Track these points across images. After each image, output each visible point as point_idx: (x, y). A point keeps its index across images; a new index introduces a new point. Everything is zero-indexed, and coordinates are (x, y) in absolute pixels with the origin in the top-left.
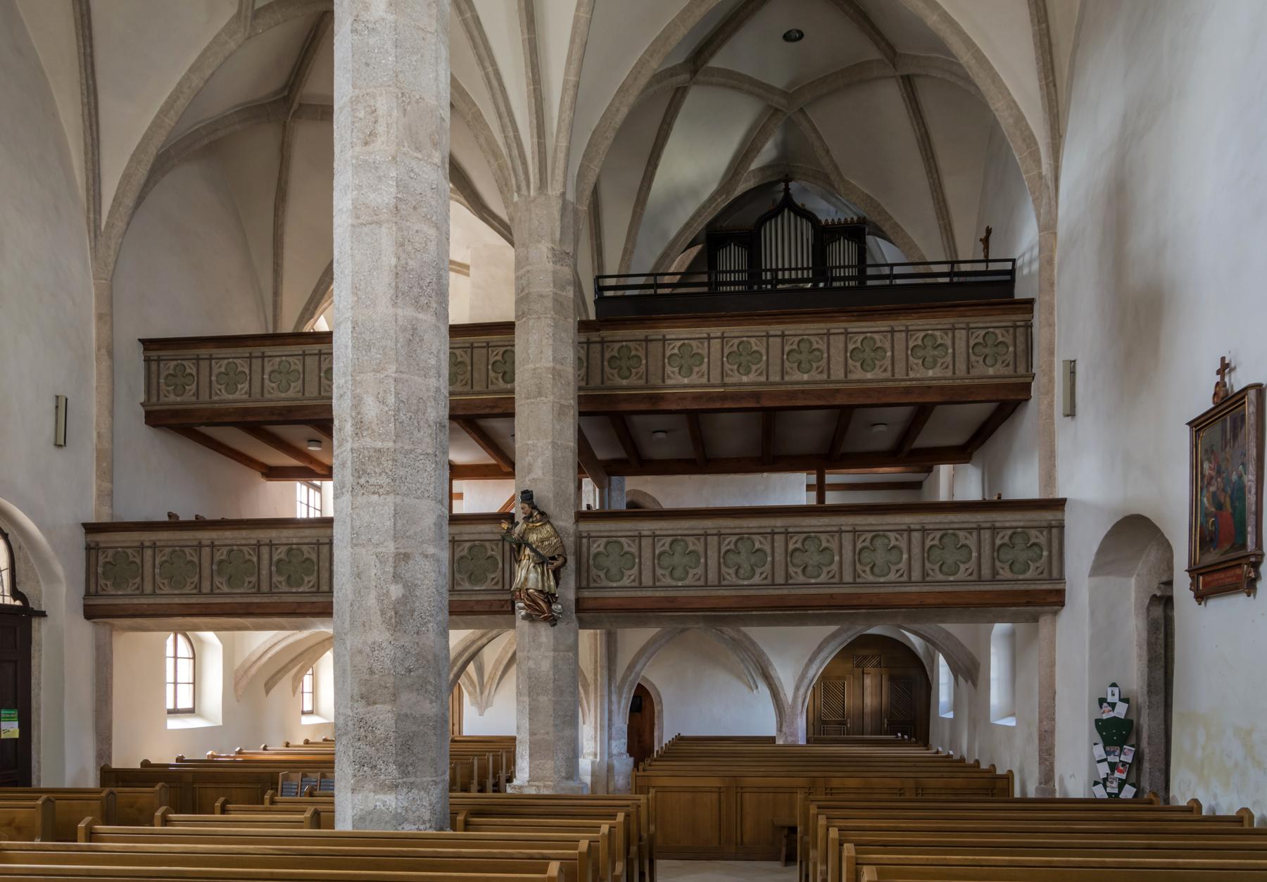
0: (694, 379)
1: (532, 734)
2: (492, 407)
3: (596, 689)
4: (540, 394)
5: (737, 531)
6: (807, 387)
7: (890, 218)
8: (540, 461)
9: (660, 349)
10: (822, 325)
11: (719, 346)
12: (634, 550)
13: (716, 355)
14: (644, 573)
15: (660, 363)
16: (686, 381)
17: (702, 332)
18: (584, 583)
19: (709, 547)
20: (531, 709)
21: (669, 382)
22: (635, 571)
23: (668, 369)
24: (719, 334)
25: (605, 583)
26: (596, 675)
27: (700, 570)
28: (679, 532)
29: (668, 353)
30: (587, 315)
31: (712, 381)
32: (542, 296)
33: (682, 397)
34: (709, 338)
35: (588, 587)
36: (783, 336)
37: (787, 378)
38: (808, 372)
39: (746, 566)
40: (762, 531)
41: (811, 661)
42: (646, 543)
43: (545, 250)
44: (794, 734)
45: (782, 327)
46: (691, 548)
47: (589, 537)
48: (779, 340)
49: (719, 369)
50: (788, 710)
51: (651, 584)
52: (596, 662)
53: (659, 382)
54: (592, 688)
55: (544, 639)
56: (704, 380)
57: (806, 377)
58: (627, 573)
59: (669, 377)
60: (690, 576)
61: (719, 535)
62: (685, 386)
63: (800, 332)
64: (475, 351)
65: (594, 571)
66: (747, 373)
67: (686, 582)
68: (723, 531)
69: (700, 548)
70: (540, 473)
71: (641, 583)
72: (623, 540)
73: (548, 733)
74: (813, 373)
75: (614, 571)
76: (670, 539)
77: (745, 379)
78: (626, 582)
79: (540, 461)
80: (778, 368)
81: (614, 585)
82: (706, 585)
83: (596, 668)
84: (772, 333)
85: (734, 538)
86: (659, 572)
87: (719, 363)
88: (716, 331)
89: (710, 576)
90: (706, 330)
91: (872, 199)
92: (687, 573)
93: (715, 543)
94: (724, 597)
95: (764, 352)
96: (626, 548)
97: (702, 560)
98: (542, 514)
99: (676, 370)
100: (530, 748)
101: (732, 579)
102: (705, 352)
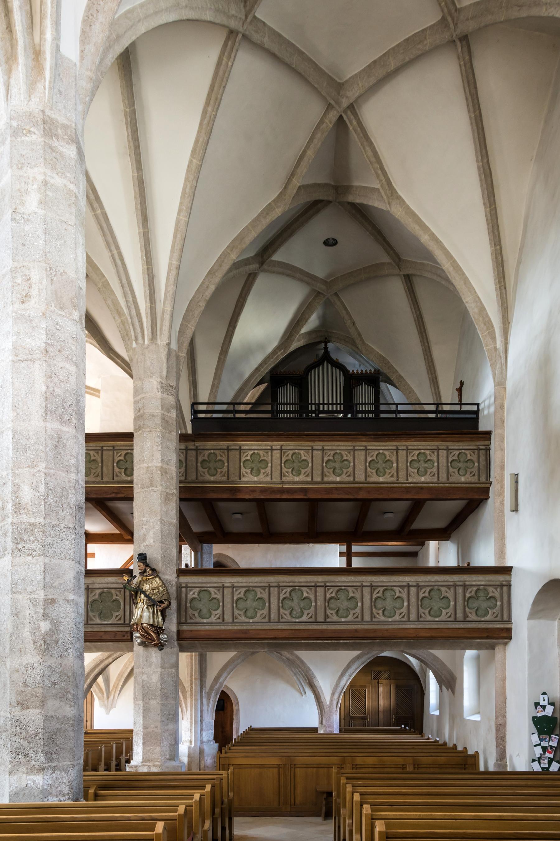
0: (261, 478)
4: (151, 485)
6: (339, 486)
8: (151, 533)
9: (238, 456)
10: (349, 444)
12: (219, 596)
14: (226, 612)
16: (256, 479)
17: (267, 445)
18: (183, 620)
20: (144, 710)
21: (244, 479)
22: (219, 611)
23: (243, 470)
25: (198, 619)
26: (191, 684)
27: (265, 611)
28: (251, 584)
32: (153, 416)
33: (253, 490)
34: (272, 450)
35: (186, 622)
36: (323, 450)
37: (326, 479)
39: (297, 608)
40: (309, 584)
43: (155, 383)
44: (331, 726)
45: (322, 444)
46: (259, 595)
47: (187, 587)
48: (320, 453)
49: (279, 472)
51: (231, 620)
52: (192, 675)
54: (188, 694)
55: (154, 660)
56: (268, 479)
57: (338, 479)
58: (214, 613)
59: (244, 476)
60: (259, 615)
63: (334, 448)
64: (104, 452)
65: (190, 612)
66: (299, 475)
68: (281, 584)
69: (265, 596)
71: (223, 619)
72: (211, 590)
73: (156, 727)
74: (344, 476)
75: (204, 611)
77: (297, 479)
78: (213, 619)
79: (151, 533)
80: (320, 472)
84: (315, 447)
86: (237, 612)
87: (279, 467)
88: (277, 445)
89: (272, 616)
91: (384, 358)
92: (256, 613)
96: (214, 595)
97: (267, 604)
99: (249, 471)
101: (288, 618)
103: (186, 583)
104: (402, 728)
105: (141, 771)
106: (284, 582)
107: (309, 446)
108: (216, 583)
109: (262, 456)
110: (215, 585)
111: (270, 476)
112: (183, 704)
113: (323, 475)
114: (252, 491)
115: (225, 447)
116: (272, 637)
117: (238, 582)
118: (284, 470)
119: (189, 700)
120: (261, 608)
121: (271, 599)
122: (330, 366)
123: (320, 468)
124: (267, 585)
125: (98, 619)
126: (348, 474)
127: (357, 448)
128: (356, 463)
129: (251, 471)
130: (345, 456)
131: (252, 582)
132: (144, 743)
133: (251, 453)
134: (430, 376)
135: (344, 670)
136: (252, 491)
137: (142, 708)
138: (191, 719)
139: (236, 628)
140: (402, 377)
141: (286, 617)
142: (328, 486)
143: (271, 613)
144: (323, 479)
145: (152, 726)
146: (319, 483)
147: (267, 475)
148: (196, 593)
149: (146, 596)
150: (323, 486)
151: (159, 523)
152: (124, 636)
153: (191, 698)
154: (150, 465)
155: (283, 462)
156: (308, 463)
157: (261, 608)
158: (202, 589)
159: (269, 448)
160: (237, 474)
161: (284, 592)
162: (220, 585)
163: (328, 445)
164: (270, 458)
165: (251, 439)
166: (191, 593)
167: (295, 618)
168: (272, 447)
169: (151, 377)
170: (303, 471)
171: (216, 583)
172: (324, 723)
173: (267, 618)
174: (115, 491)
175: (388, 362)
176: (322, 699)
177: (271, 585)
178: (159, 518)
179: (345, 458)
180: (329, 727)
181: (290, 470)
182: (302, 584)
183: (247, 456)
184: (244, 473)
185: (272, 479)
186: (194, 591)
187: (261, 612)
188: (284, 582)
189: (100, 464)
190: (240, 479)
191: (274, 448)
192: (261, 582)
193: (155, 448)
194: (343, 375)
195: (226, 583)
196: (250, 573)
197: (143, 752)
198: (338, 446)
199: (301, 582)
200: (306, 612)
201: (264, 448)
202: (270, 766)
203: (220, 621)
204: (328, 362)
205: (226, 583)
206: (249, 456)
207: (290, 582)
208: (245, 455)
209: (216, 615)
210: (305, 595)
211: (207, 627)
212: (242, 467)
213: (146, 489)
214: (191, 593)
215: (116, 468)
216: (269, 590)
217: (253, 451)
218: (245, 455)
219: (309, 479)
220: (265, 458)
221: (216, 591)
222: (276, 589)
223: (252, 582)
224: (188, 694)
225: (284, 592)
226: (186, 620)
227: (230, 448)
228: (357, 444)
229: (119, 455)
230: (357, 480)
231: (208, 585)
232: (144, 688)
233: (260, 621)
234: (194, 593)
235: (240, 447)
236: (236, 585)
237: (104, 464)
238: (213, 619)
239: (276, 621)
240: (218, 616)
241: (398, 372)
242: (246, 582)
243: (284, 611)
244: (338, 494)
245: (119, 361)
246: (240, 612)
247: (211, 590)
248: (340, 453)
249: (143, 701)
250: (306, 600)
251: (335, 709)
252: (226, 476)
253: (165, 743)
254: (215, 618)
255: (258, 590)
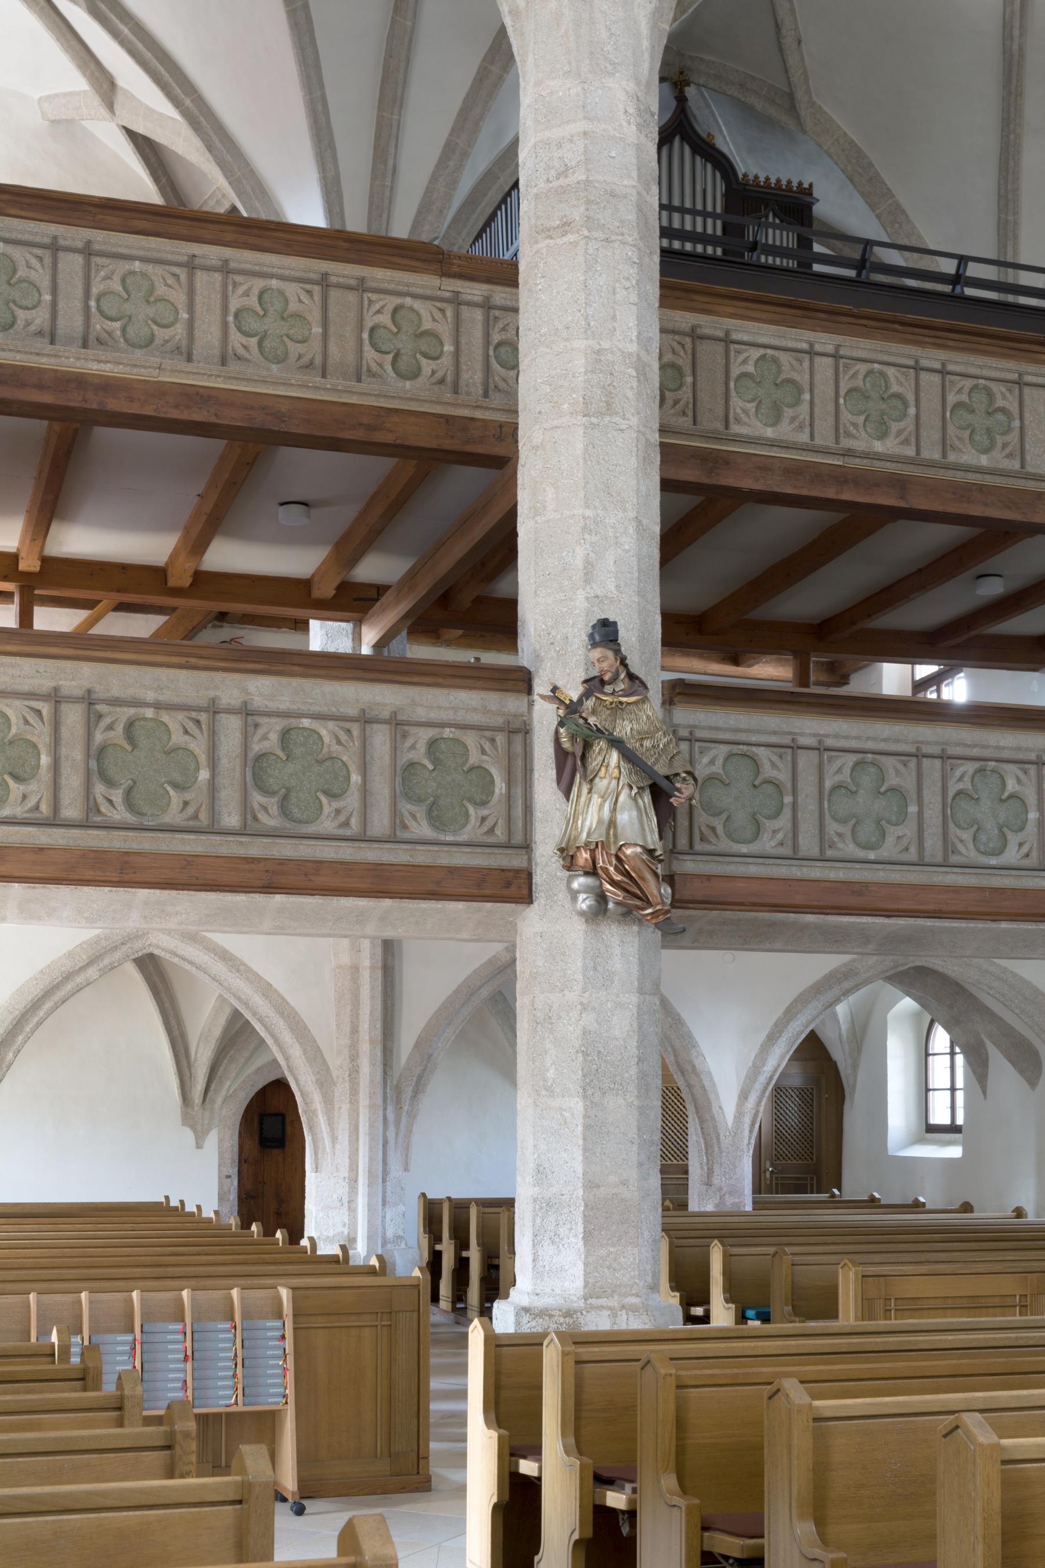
0: (784, 431)
1: (590, 1185)
2: (370, 428)
3: (354, 1092)
4: (609, 409)
5: (976, 752)
6: (989, 480)
7: (890, 194)
8: (610, 558)
9: (720, 360)
10: (1011, 364)
11: (830, 373)
12: (783, 776)
13: (825, 390)
14: (803, 827)
15: (720, 390)
16: (769, 433)
17: (799, 337)
18: (683, 842)
19: (926, 783)
20: (587, 1127)
21: (735, 428)
22: (784, 821)
23: (737, 403)
24: (830, 349)
25: (725, 844)
26: (354, 1058)
27: (908, 830)
28: (870, 745)
29: (735, 371)
30: (1005, 254)
31: (819, 441)
32: (613, 194)
33: (765, 466)
34: (812, 353)
35: (691, 850)
36: (943, 372)
37: (952, 457)
38: (986, 451)
39: (990, 825)
40: (1021, 756)
41: (772, 1038)
42: (806, 761)
43: (621, 95)
44: (735, 1191)
45: (942, 355)
46: (892, 780)
47: (691, 740)
48: (936, 378)
49: (831, 420)
50: (726, 1142)
51: (815, 852)
52: (355, 1030)
53: (719, 426)
54: (341, 1090)
55: (617, 965)
56: (804, 437)
57: (984, 460)
58: (770, 825)
59: (738, 421)
60: (890, 840)
61: (943, 757)
62: (772, 444)
63: (972, 371)
64: (334, 293)
65: (702, 818)
66: (883, 436)
67: (884, 853)
68: (951, 751)
69: (909, 783)
70: (611, 586)
71: (795, 847)
72: (762, 752)
73: (624, 1183)
74: (997, 454)
75: (741, 818)
76: (853, 758)
77: (878, 447)
78: (767, 844)
79: (610, 558)
80: (937, 436)
81: (744, 849)
82: (921, 863)
83: (354, 1046)
84: (924, 363)
85: (971, 767)
86: (832, 827)
87: (831, 407)
88: (826, 342)
89: (928, 843)
90: (808, 335)
91: (859, 151)
92: (883, 835)
93: (937, 775)
94: (957, 890)
95: (911, 397)
96: (768, 772)
97: (913, 809)
98: (632, 677)
99: (751, 406)
100: (587, 1220)
101: (969, 853)
102: (804, 379)
103: (692, 728)
104: (833, 1195)
105: (592, 1327)
106: (957, 744)
107: (909, 357)
108: (775, 733)
109: (786, 367)
110: (773, 739)
111: (807, 430)
112: (322, 1120)
113: (945, 446)
114: (760, 468)
115: (685, 326)
116: (931, 907)
117: (836, 736)
118: (846, 416)
119: (344, 1109)
120: (894, 818)
121: (926, 792)
122: (687, 150)
123: (938, 423)
124: (912, 749)
125: (424, 823)
126: (1007, 451)
127: (1028, 378)
128: (1027, 422)
129: (757, 408)
130: (999, 396)
131: (874, 739)
132: (588, 1236)
133: (756, 353)
134: (1011, 218)
135: (776, 1025)
136: (760, 468)
137: (580, 1121)
138: (353, 1167)
139: (832, 875)
140: (903, 212)
141: (963, 850)
142: (959, 476)
143: (926, 834)
144: (944, 455)
145: (613, 1179)
146: (931, 464)
147: (801, 427)
148: (719, 762)
149: (628, 756)
150: (949, 475)
151: (631, 531)
152: (508, 885)
153: (354, 1101)
154: (606, 344)
155: (842, 393)
156: (906, 404)
157: (894, 818)
158: (736, 749)
159: (805, 346)
160: (720, 410)
161: (958, 773)
162: (786, 740)
163: (960, 361)
164: (807, 377)
165: (758, 315)
166: (705, 760)
167: (984, 853)
168: (811, 345)
169: (611, 74)
170: (895, 427)
171: (775, 733)
172: (716, 1180)
173: (913, 850)
174: (365, 421)
175: (871, 164)
176: (715, 1109)
177: (925, 749)
178: (632, 514)
179: (1000, 403)
180: (730, 1193)
181: (862, 418)
182: (1006, 754)
183: (745, 362)
184: (738, 411)
185: (812, 437)
186: (712, 753)
187: (899, 831)
188: (957, 744)
189: (317, 330)
190: (727, 427)
191: (818, 348)
192: (897, 741)
193: (621, 294)
194: (722, 178)
195: (802, 734)
196: (841, 707)
197: (586, 1265)
198: (981, 367)
199: (1004, 748)
200: (1013, 839)
201: (790, 344)
202: (997, 1301)
203: (786, 851)
204: (682, 139)
205: (802, 734)
206: (751, 362)
207: (975, 746)
208: (741, 358)
209: (775, 832)
210: (1011, 786)
211: (754, 869)
212: (733, 393)
213: (594, 420)
214: (705, 760)
215: (367, 347)
216: (919, 766)
217: (762, 351)
218: (741, 358)
219: (910, 452)
220: (795, 376)
221: (774, 758)
222: (938, 763)
223: (874, 739)
224: (341, 1090)
225: (958, 773)
226: (691, 846)
227: (699, 331)
228: (1032, 368)
229: (377, 306)
230: (1029, 469)
231: (754, 739)
232: (586, 1054)
233: (896, 857)
234: (712, 762)
235: (727, 333)
236: (829, 742)
237: (332, 329)
238: (767, 844)
239: (939, 859)
240: (780, 836)
241: (893, 196)
242: (858, 738)
243: (959, 832)
244: (986, 505)
245: (126, 31)
246: (841, 829)
247: (762, 752)
248: (986, 389)
249: (585, 1097)
250: (1011, 802)
251: (746, 1141)
252: (690, 413)
253: (646, 1234)
254: (773, 844)
255: (889, 762)
